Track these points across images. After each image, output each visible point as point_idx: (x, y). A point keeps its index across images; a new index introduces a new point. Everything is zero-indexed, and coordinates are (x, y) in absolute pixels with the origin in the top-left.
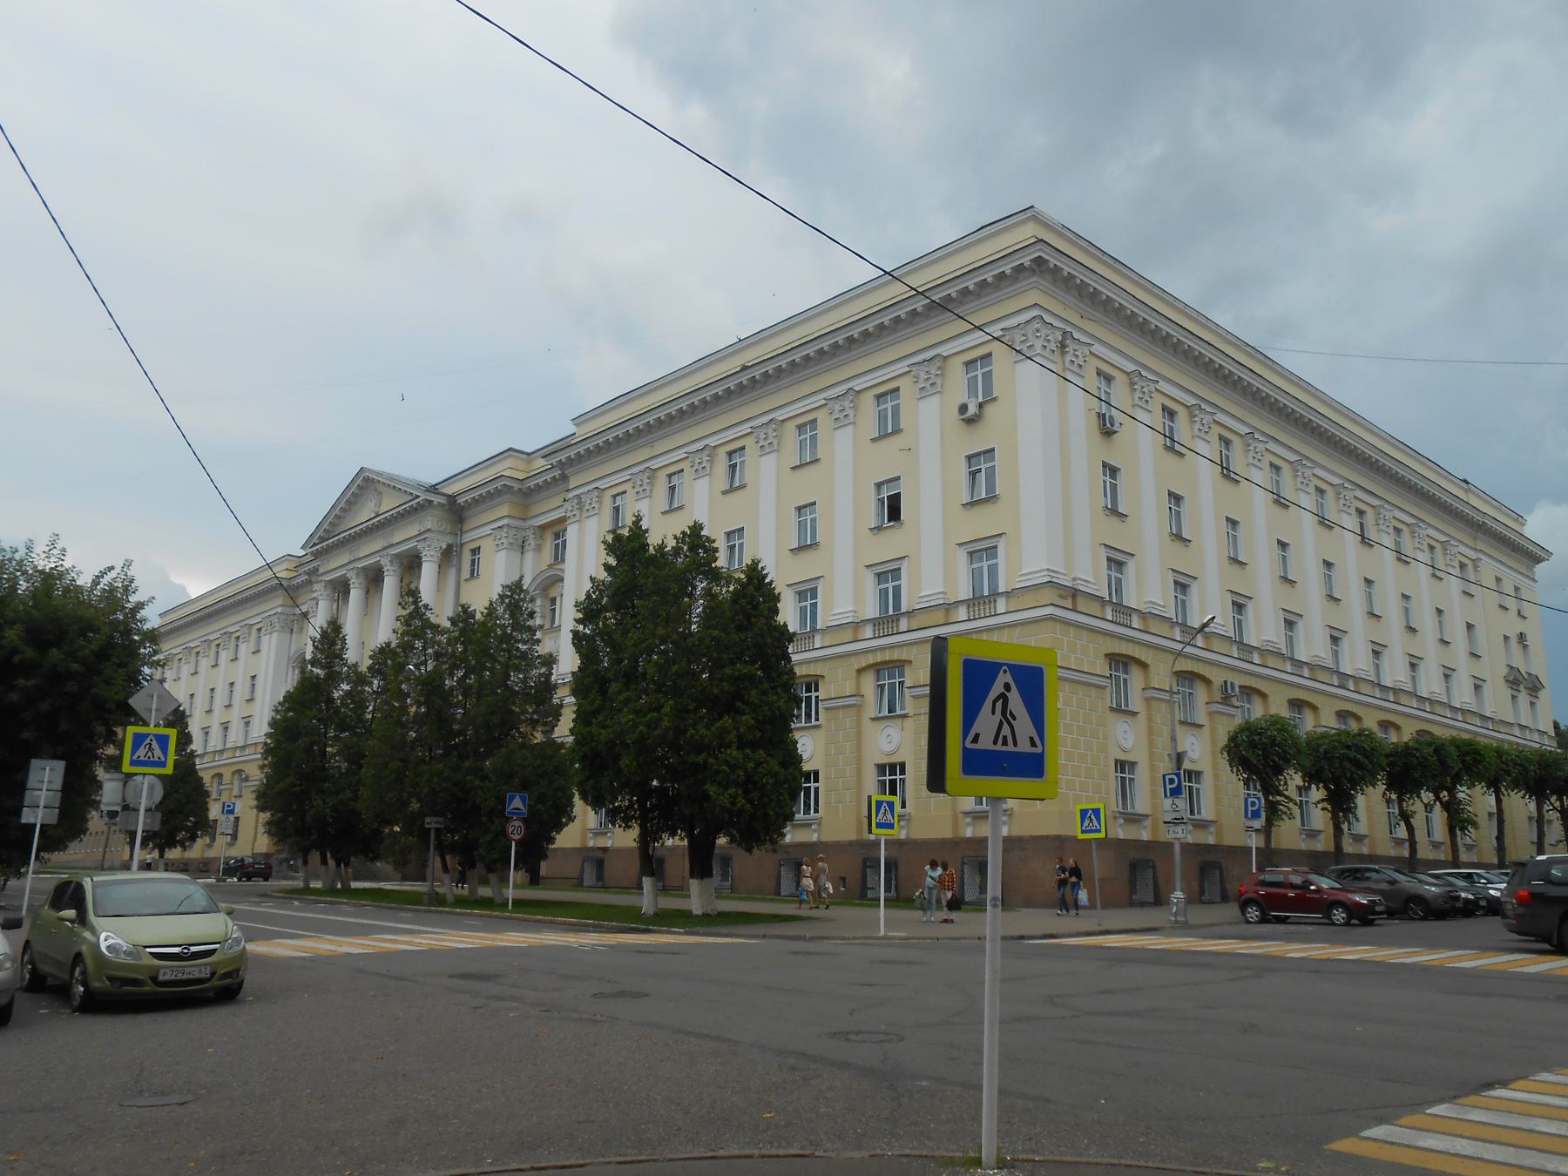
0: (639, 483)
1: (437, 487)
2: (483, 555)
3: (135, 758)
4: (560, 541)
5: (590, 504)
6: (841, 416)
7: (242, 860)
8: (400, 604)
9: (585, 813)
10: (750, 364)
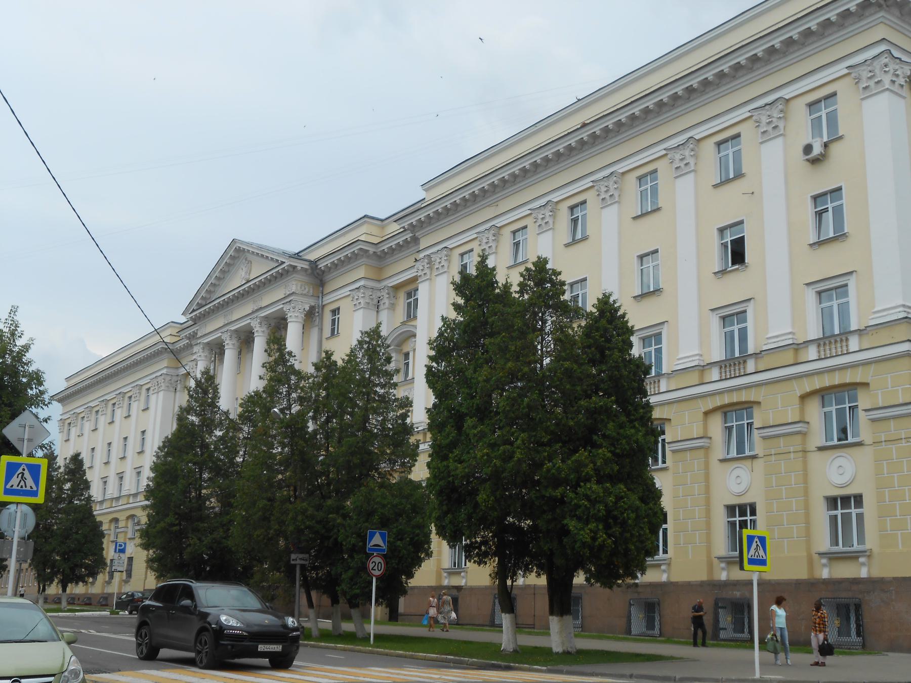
0: (485, 241)
1: (300, 254)
2: (342, 316)
3: (8, 487)
4: (412, 300)
5: (440, 263)
7: (133, 595)
8: (266, 351)
9: (440, 546)
10: (588, 122)
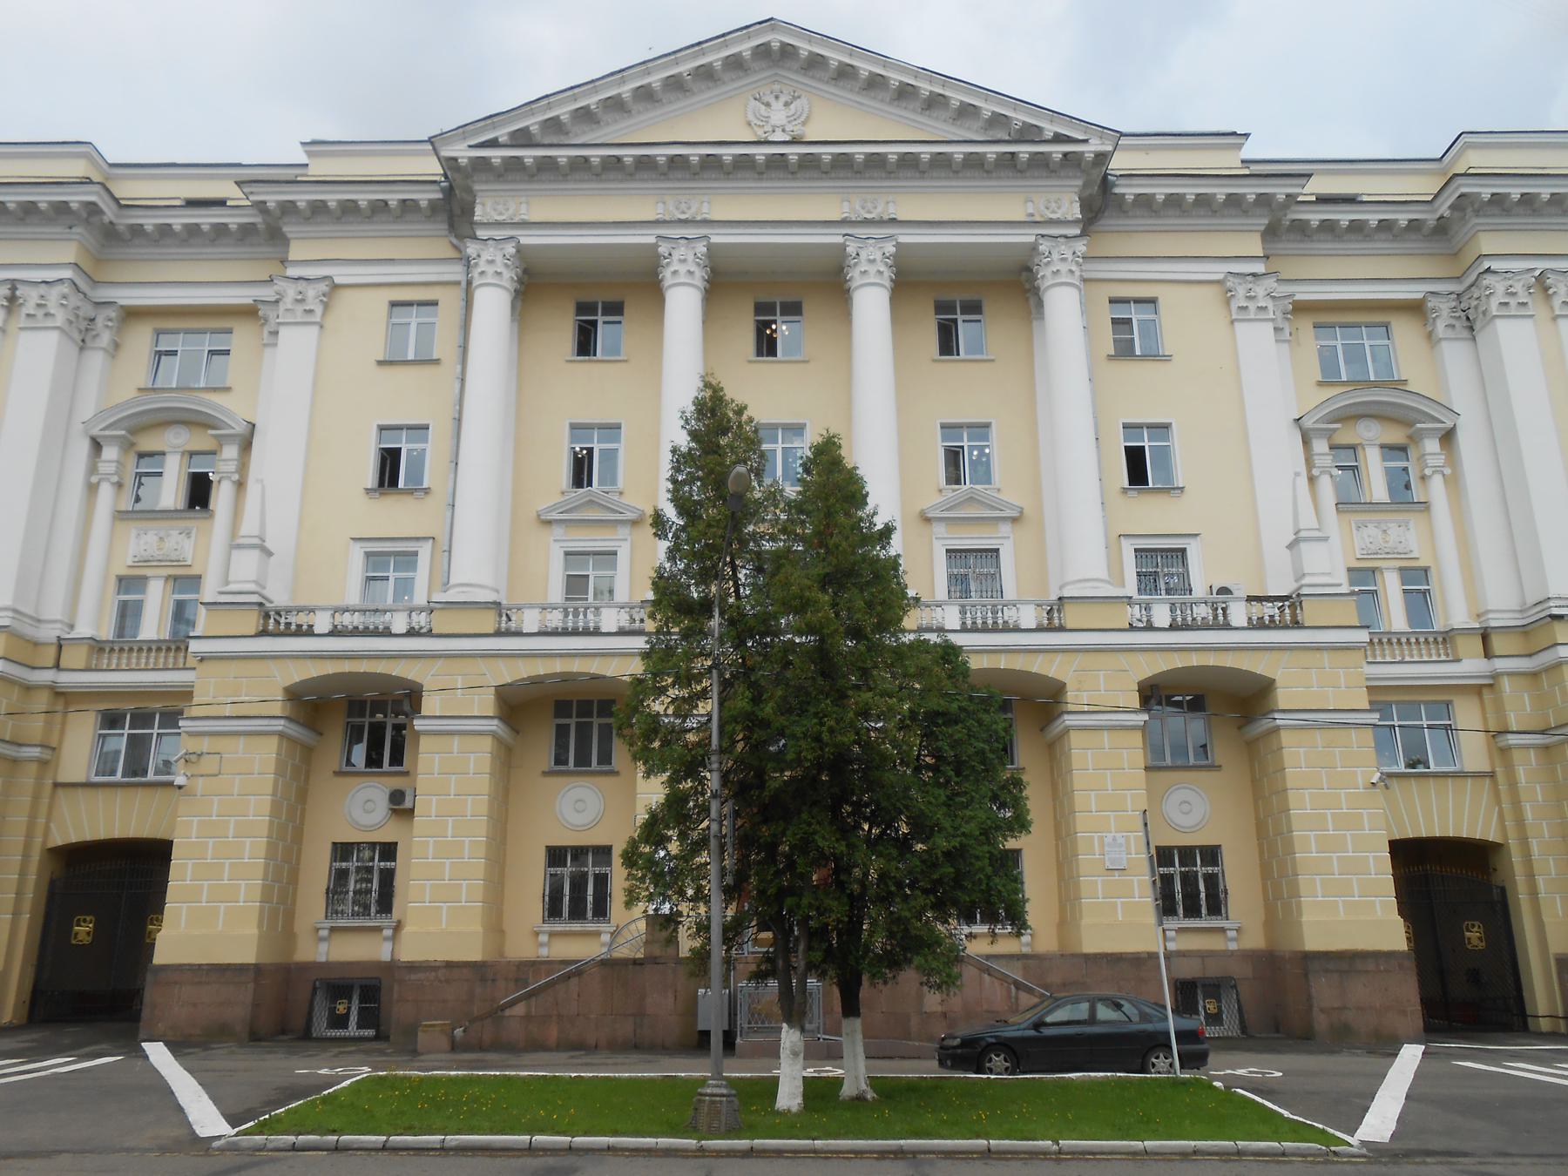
6: (1513, 302)
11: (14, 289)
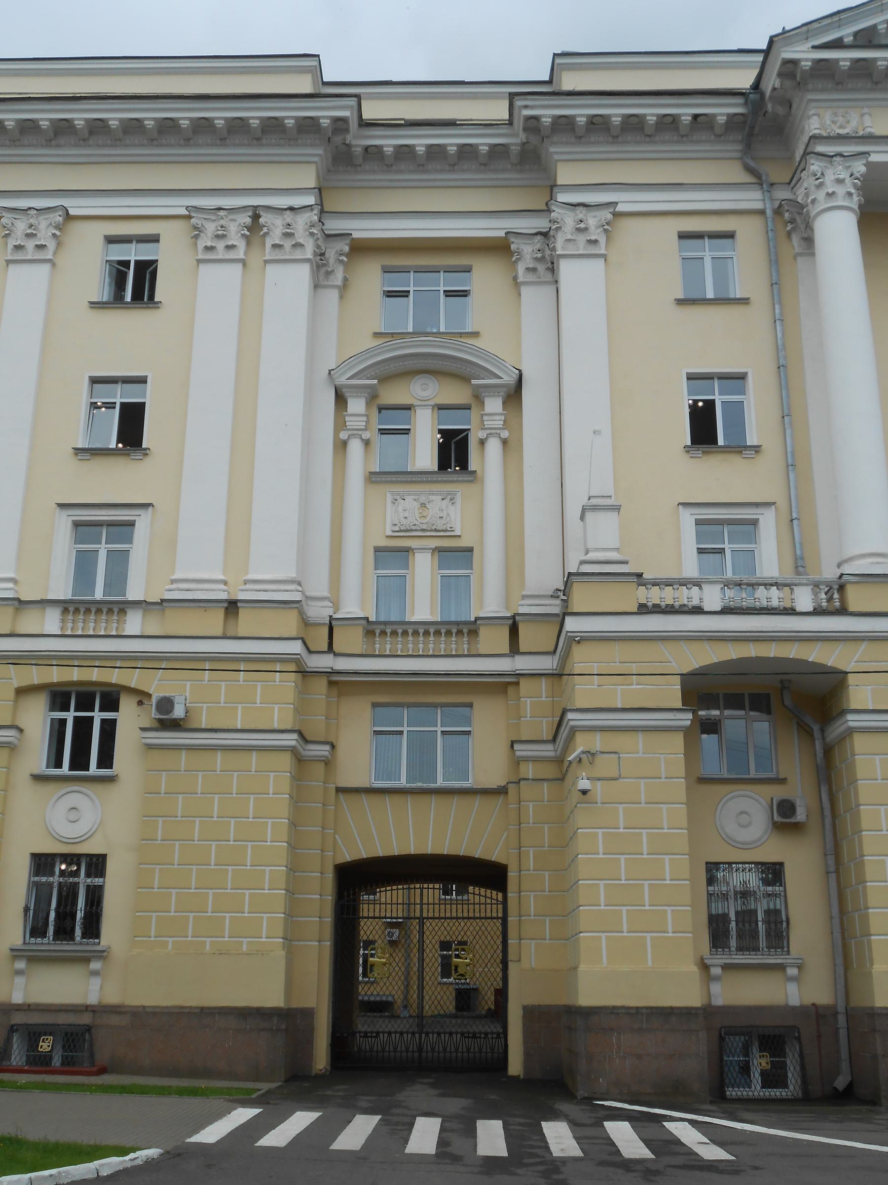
11: (256, 217)
